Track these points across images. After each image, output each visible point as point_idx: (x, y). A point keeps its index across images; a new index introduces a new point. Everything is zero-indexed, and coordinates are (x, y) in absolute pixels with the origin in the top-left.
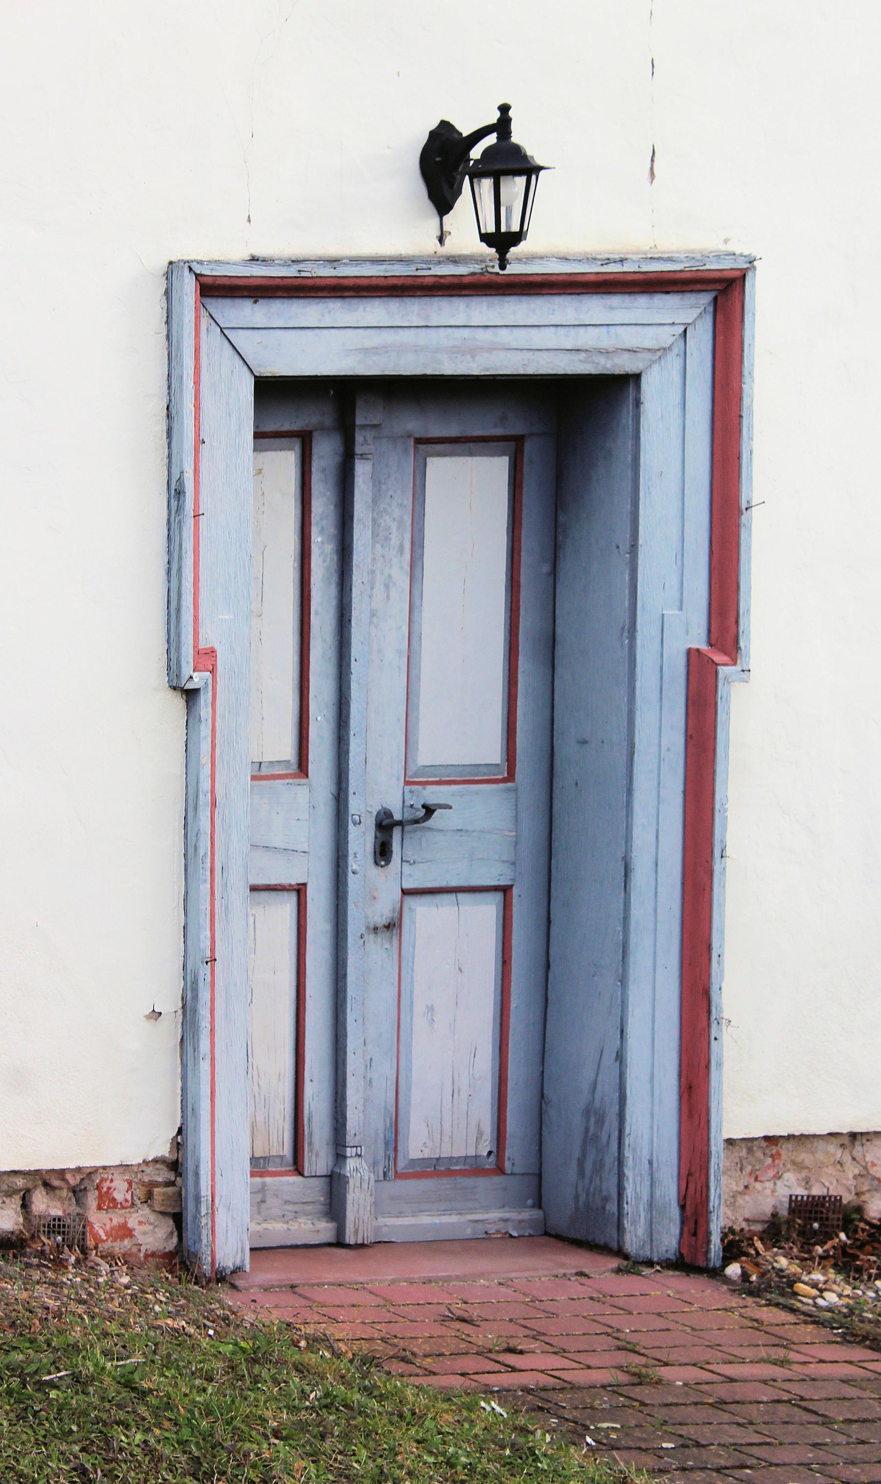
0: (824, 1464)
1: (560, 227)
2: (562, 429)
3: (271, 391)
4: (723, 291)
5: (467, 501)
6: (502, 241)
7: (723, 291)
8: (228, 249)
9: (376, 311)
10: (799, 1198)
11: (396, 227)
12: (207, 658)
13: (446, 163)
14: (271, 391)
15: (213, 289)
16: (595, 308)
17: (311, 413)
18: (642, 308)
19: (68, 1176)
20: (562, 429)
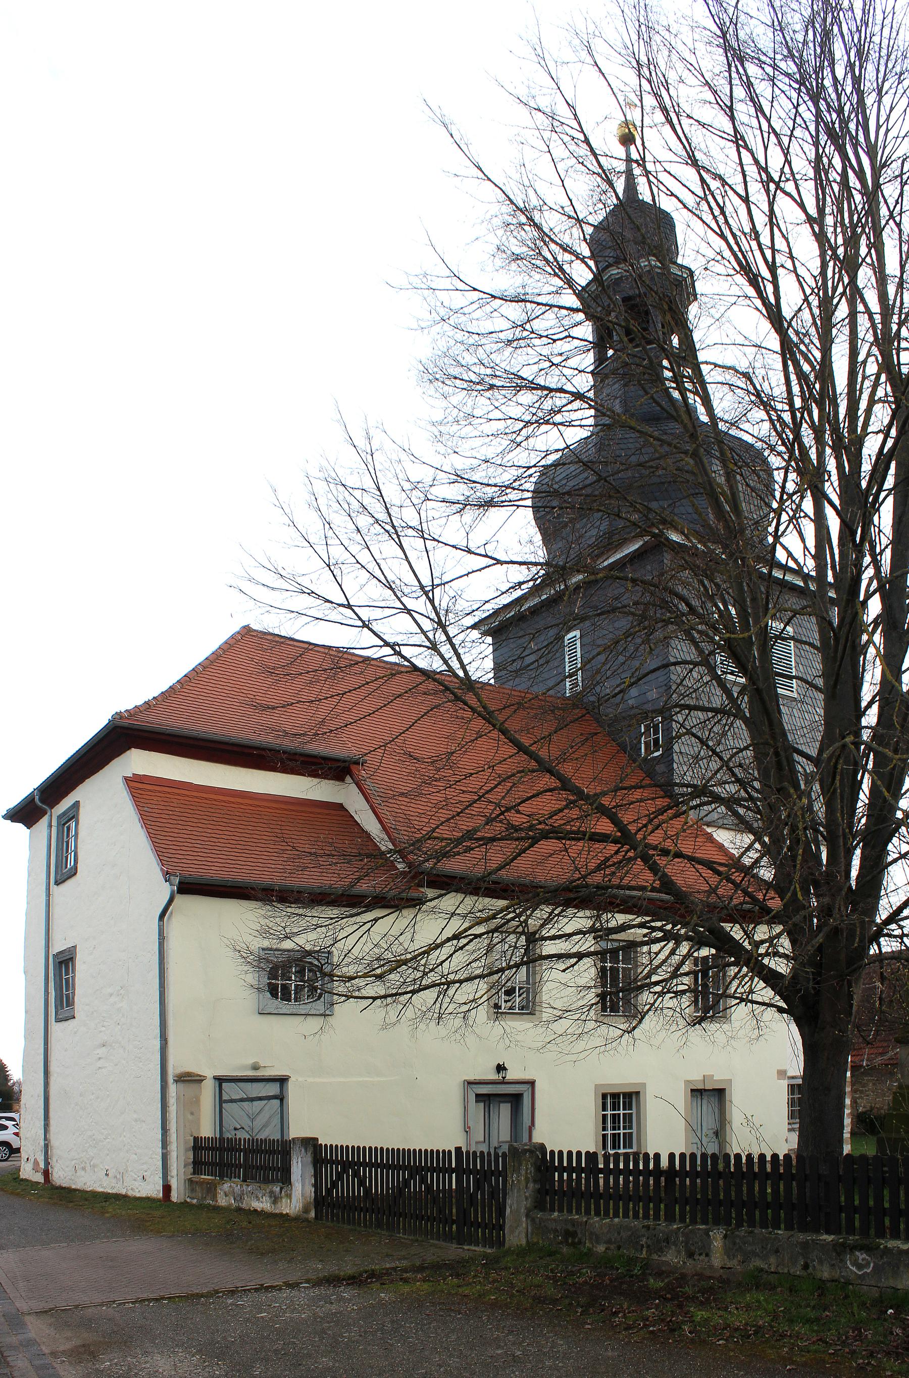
0: (457, 698)
1: (511, 1075)
2: (515, 1100)
3: (477, 1095)
4: (532, 1083)
5: (505, 1110)
6: (504, 1078)
7: (532, 1083)
8: (471, 1077)
9: (490, 1086)
10: (664, 1163)
11: (493, 1076)
12: (469, 1128)
13: (500, 1068)
14: (477, 1095)
15: (470, 1083)
16: (517, 1086)
17: (479, 1097)
18: (522, 1086)
19: (713, 657)
20: (515, 1100)
